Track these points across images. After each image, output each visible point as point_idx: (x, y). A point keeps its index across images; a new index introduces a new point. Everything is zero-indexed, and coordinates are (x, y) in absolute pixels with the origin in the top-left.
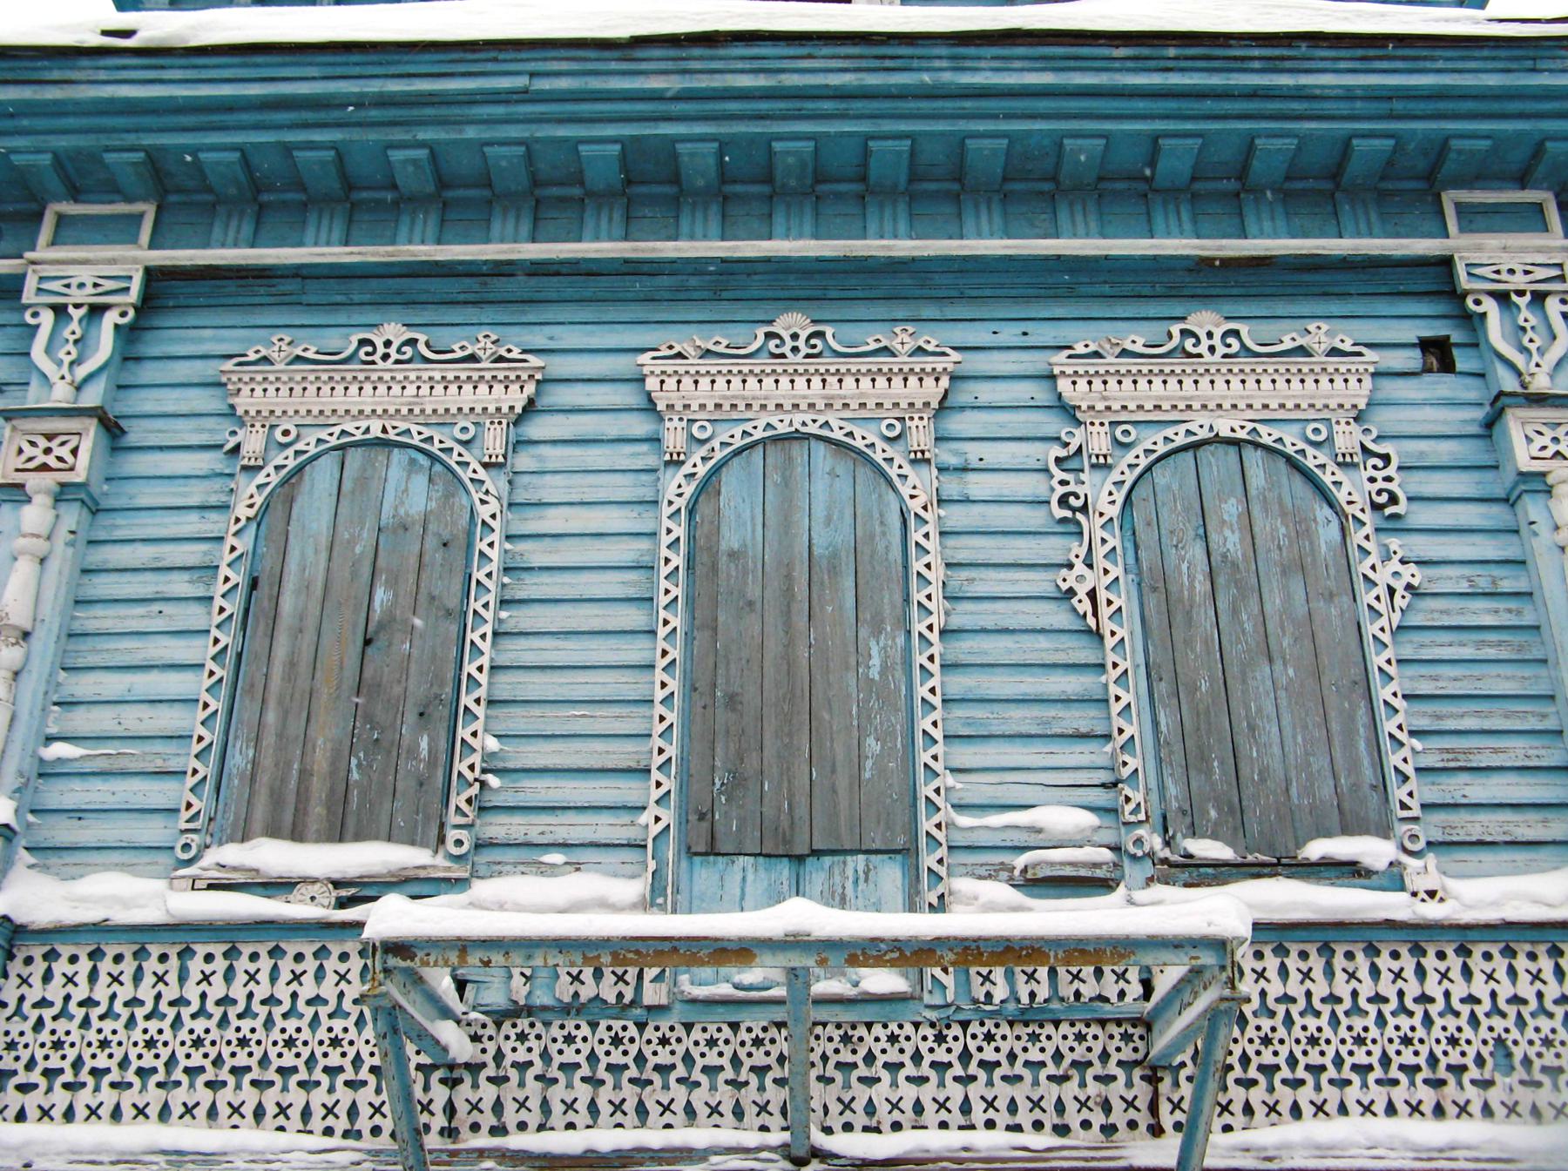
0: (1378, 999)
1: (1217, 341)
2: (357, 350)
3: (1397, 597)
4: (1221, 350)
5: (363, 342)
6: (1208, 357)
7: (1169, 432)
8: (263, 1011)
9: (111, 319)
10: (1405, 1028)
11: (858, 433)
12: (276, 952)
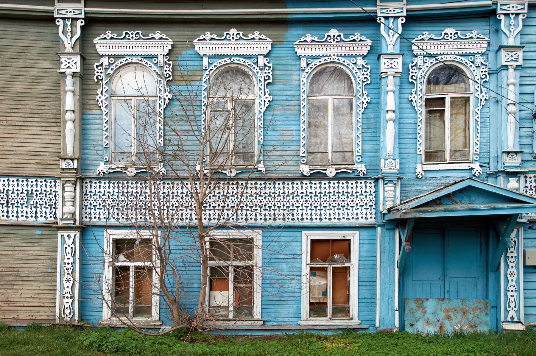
0: (366, 192)
1: (235, 36)
2: (125, 36)
3: (266, 103)
4: (235, 38)
5: (227, 34)
6: (232, 40)
7: (122, 60)
8: (16, 192)
9: (521, 17)
10: (343, 199)
11: (346, 61)
12: (118, 183)
